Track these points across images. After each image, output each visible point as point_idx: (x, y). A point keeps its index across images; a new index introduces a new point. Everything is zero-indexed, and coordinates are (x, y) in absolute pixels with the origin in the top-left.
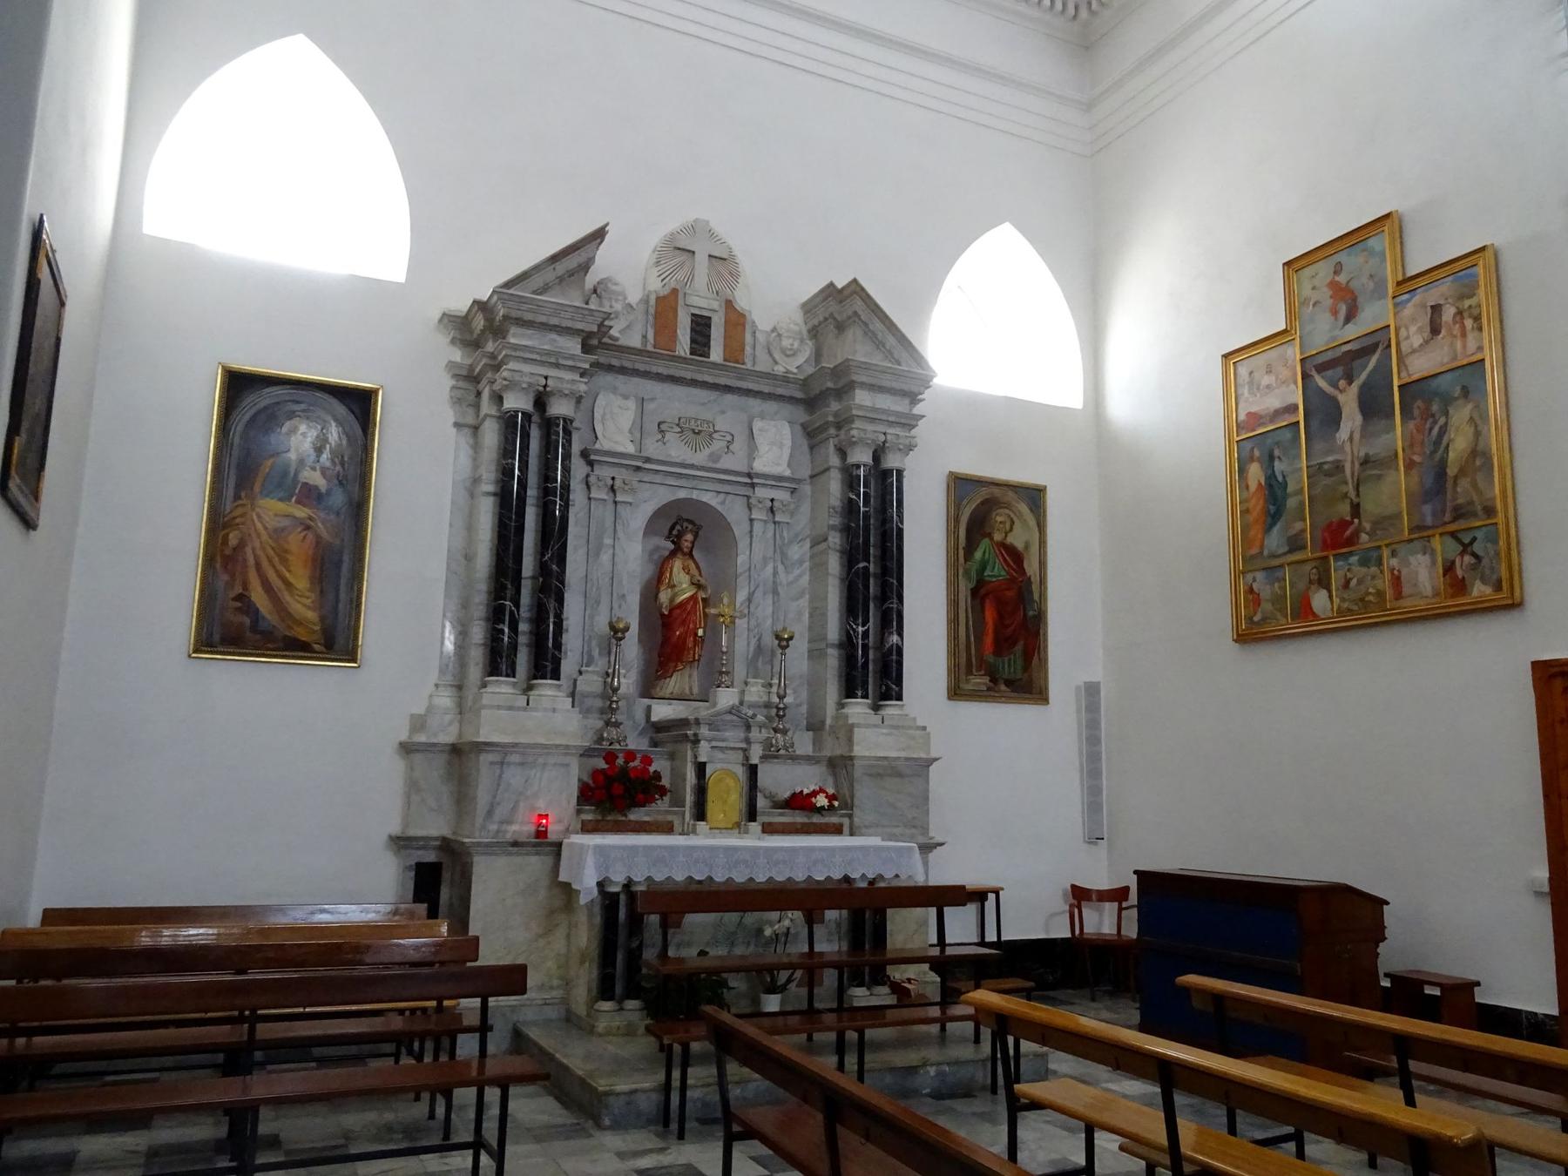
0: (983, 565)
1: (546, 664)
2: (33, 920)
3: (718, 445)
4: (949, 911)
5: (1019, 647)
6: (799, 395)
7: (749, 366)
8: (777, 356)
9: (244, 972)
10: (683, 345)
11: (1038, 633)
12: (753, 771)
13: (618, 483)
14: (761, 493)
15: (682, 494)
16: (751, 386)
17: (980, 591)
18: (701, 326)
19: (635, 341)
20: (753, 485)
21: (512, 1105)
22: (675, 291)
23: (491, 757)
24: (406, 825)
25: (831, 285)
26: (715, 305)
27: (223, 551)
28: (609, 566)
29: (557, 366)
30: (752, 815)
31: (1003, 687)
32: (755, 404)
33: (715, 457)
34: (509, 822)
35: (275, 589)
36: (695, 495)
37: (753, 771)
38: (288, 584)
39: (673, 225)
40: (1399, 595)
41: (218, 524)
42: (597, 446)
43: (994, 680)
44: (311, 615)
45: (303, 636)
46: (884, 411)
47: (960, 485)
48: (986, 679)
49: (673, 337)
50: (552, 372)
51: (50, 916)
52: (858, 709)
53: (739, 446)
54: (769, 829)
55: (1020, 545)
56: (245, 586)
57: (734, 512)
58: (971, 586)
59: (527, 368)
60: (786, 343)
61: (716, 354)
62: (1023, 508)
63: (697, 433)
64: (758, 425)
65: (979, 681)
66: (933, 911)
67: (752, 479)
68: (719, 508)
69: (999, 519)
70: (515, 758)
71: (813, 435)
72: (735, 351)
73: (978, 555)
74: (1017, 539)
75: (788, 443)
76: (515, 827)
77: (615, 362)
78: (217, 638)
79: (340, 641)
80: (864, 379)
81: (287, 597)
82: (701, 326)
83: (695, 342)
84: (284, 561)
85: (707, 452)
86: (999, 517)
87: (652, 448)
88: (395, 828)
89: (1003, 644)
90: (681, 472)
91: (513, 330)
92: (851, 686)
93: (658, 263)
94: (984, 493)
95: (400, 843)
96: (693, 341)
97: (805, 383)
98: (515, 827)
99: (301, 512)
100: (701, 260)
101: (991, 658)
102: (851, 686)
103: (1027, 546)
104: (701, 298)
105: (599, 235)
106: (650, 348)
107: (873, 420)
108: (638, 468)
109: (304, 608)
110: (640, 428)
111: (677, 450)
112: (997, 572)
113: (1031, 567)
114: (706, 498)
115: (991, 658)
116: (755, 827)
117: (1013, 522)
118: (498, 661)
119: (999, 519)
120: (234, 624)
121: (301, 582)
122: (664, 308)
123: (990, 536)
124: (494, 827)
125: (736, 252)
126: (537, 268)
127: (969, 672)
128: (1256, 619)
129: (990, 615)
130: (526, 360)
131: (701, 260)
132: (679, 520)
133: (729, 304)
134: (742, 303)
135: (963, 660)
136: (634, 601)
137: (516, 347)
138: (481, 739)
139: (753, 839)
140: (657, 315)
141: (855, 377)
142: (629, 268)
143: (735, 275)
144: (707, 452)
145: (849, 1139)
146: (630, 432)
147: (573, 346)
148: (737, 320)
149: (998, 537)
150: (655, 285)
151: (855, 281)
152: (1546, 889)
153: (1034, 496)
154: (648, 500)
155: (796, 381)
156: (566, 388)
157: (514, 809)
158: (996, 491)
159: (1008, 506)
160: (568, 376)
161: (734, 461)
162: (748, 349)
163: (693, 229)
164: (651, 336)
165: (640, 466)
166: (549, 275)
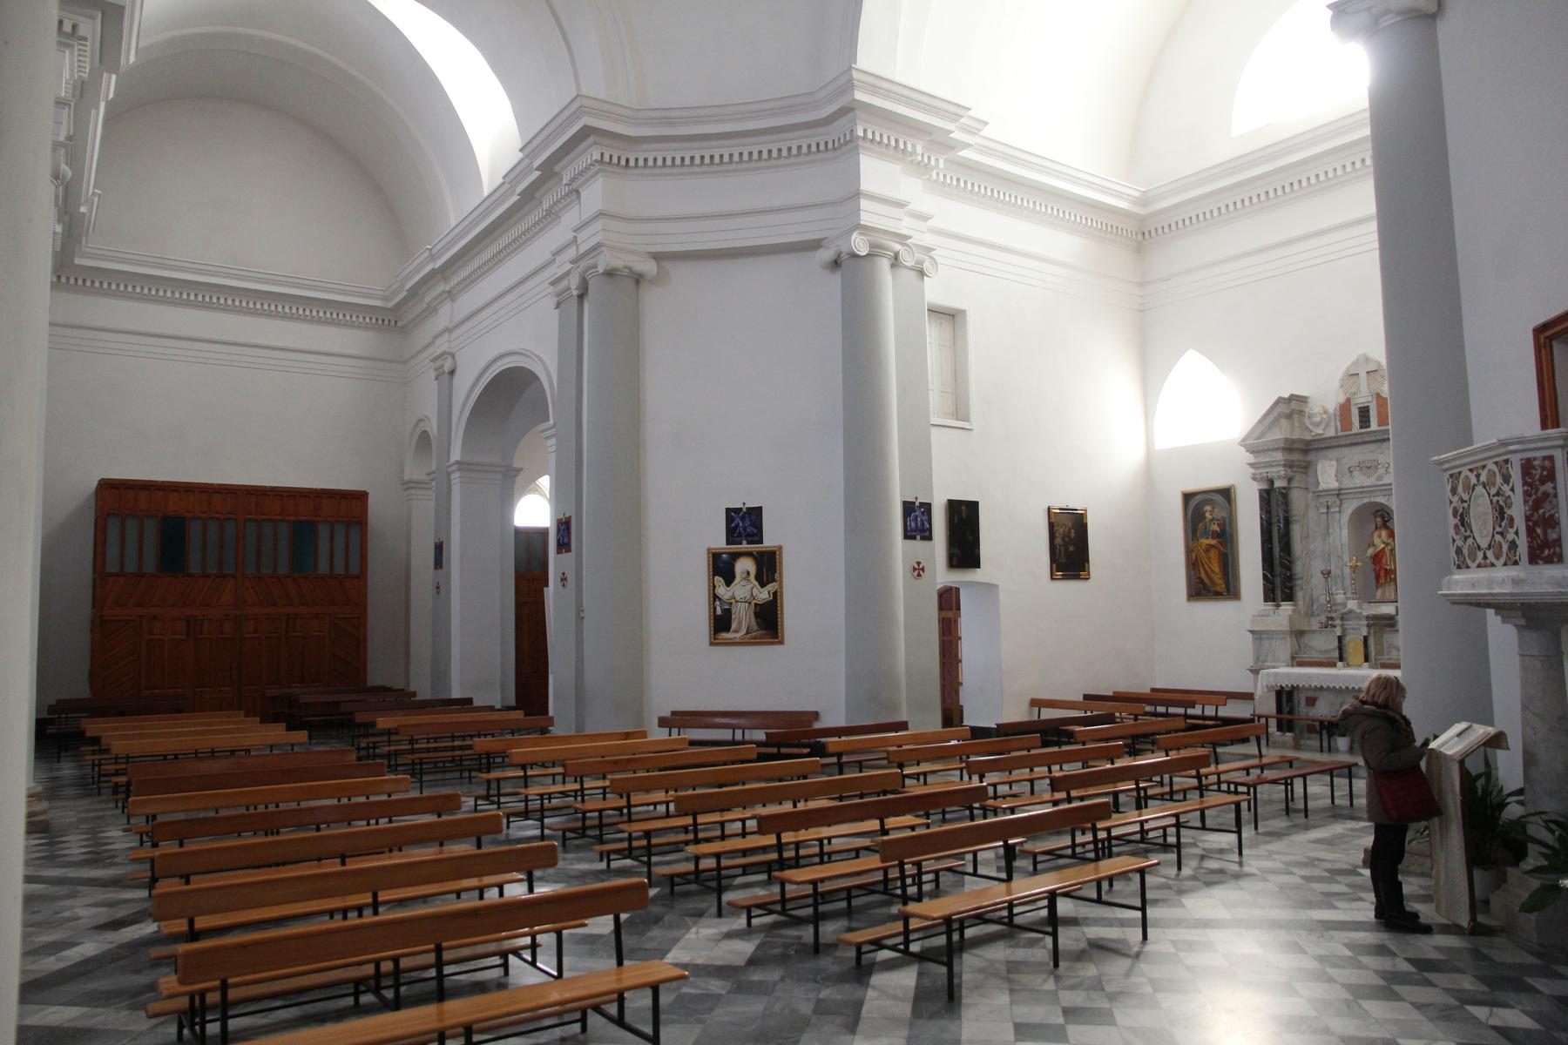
1: (1289, 597)
3: (1381, 471)
9: (805, 777)
10: (1356, 427)
18: (1364, 413)
19: (1331, 433)
21: (1309, 790)
22: (1348, 400)
25: (288, 729)
27: (1193, 564)
28: (1327, 546)
35: (1210, 576)
41: (1189, 551)
49: (1351, 423)
61: (1374, 426)
63: (1368, 468)
82: (1364, 413)
87: (1347, 483)
90: (1363, 491)
99: (1213, 542)
100: (1363, 375)
109: (1218, 579)
111: (1360, 480)
114: (1378, 500)
120: (1200, 589)
121: (1217, 569)
122: (1345, 408)
128: (560, 770)
147: (1279, 456)
150: (1342, 399)
151: (975, 504)
152: (911, 995)
154: (1350, 507)
163: (1355, 363)
165: (1339, 493)
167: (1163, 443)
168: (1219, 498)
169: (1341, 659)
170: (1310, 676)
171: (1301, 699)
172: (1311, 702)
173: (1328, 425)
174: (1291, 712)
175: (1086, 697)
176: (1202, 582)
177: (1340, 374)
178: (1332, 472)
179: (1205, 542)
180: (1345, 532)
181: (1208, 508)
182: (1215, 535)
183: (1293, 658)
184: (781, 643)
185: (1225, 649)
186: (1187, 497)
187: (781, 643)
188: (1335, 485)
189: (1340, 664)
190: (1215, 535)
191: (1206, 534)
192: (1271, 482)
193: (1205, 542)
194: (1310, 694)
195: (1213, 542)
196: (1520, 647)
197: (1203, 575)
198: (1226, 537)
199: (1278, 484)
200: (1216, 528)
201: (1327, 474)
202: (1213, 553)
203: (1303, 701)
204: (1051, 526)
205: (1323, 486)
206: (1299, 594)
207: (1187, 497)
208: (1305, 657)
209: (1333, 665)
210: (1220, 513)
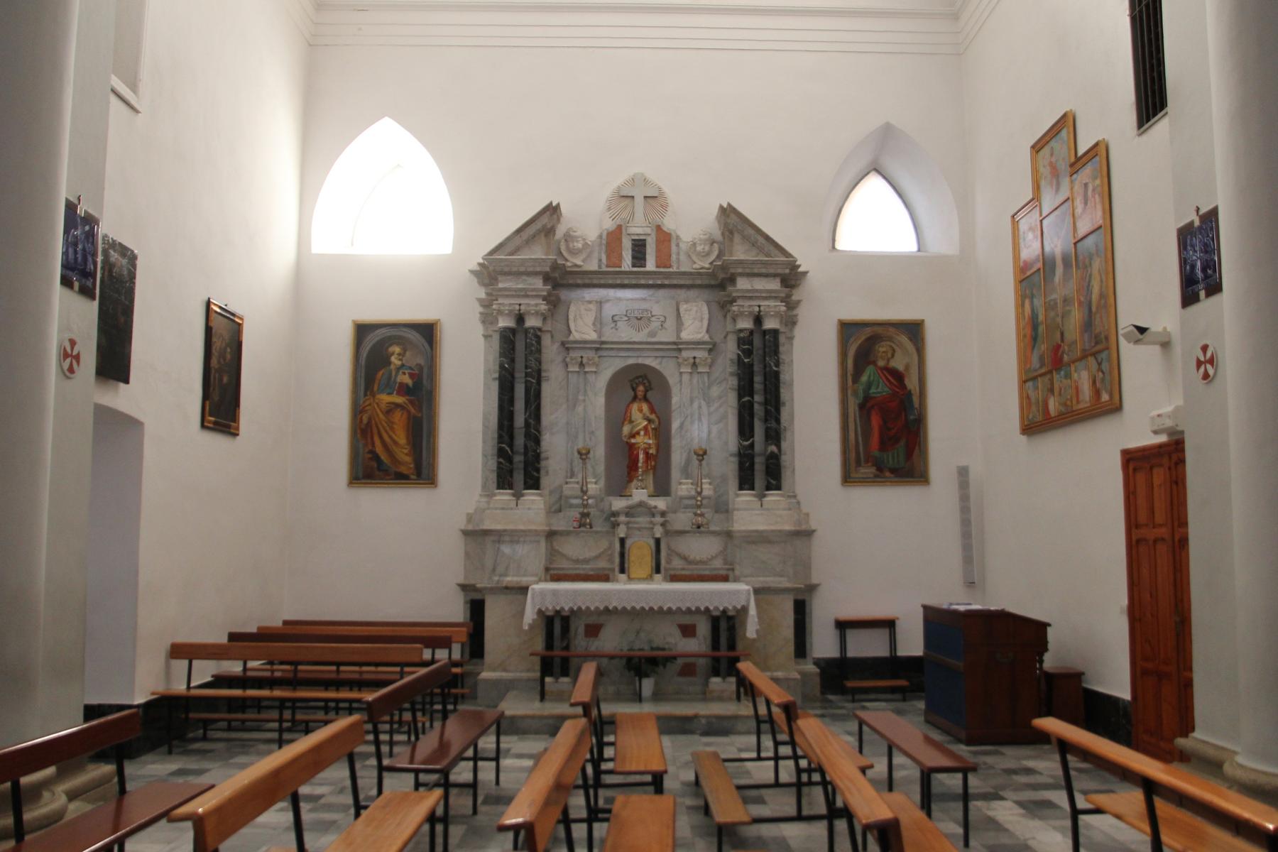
0: (869, 385)
1: (533, 483)
2: (280, 624)
3: (655, 324)
4: (195, 662)
5: (902, 443)
6: (713, 282)
7: (674, 269)
8: (694, 258)
10: (627, 263)
11: (918, 429)
12: (658, 541)
13: (585, 361)
14: (685, 354)
15: (631, 361)
16: (675, 282)
17: (866, 405)
18: (639, 248)
19: (592, 266)
20: (680, 350)
22: (619, 227)
23: (492, 538)
24: (466, 577)
26: (648, 231)
27: (364, 429)
28: (576, 417)
29: (527, 296)
30: (658, 571)
31: (888, 474)
32: (682, 293)
33: (652, 334)
34: (506, 575)
36: (640, 361)
37: (658, 541)
38: (395, 443)
39: (619, 181)
40: (1078, 402)
41: (357, 411)
42: (571, 338)
43: (880, 469)
44: (408, 459)
45: (403, 469)
46: (757, 291)
47: (847, 329)
48: (873, 470)
49: (620, 257)
50: (522, 301)
51: (286, 623)
52: (746, 497)
53: (670, 323)
54: (674, 578)
55: (901, 368)
56: (373, 444)
57: (667, 368)
58: (861, 400)
59: (507, 301)
60: (699, 248)
61: (651, 265)
62: (904, 339)
64: (683, 307)
65: (869, 470)
66: (186, 662)
67: (677, 347)
68: (658, 367)
69: (882, 350)
70: (507, 538)
71: (725, 306)
72: (663, 260)
73: (864, 378)
74: (898, 363)
75: (706, 316)
76: (509, 579)
77: (579, 281)
78: (360, 475)
79: (425, 471)
80: (740, 270)
81: (395, 449)
82: (639, 248)
83: (638, 257)
84: (392, 429)
85: (646, 331)
86: (882, 348)
87: (609, 335)
88: (461, 580)
89: (887, 443)
90: (630, 347)
91: (500, 278)
92: (746, 482)
93: (609, 209)
94: (868, 332)
95: (464, 587)
96: (634, 257)
97: (713, 275)
98: (509, 579)
99: (400, 400)
100: (639, 200)
101: (876, 453)
102: (746, 482)
103: (907, 367)
104: (639, 227)
105: (208, 303)
106: (604, 269)
107: (750, 298)
108: (597, 349)
109: (404, 455)
110: (598, 323)
111: (626, 333)
112: (881, 389)
113: (912, 383)
114: (648, 362)
115: (876, 453)
116: (658, 577)
117: (894, 351)
118: (504, 480)
119: (882, 350)
121: (402, 440)
122: (613, 239)
123: (874, 363)
124: (496, 578)
125: (666, 189)
126: (508, 239)
127: (858, 463)
129: (875, 421)
130: (507, 296)
131: (639, 200)
132: (645, 377)
133: (659, 228)
134: (669, 224)
135: (853, 455)
136: (601, 434)
137: (501, 290)
138: (485, 527)
139: (659, 585)
140: (608, 244)
141: (732, 271)
142: (587, 219)
143: (665, 207)
144: (646, 331)
145: (1159, 803)
146: (594, 324)
147: (538, 283)
148: (664, 238)
149: (881, 363)
150: (609, 225)
153: (914, 330)
154: (611, 367)
155: (707, 274)
156: (533, 310)
157: (507, 568)
158: (879, 330)
159: (890, 339)
160: (533, 302)
161: (667, 336)
162: (674, 257)
163: (632, 181)
164: (604, 260)
165: (599, 347)
166: (518, 241)
167: (323, 244)
168: (414, 336)
169: (622, 571)
170: (720, 594)
171: (578, 627)
172: (593, 631)
173: (589, 256)
174: (567, 648)
175: (233, 637)
176: (376, 458)
177: (607, 192)
178: (589, 318)
179: (385, 398)
180: (601, 400)
181: (397, 349)
182: (403, 390)
183: (547, 569)
184: (923, 321)
185: (395, 559)
186: (362, 330)
187: (923, 321)
188: (593, 336)
189: (623, 576)
190: (403, 390)
191: (389, 387)
192: (520, 319)
193: (385, 398)
194: (593, 620)
195: (400, 400)
196: (1187, 534)
197: (379, 449)
198: (421, 394)
199: (531, 322)
200: (406, 379)
201: (585, 317)
202: (398, 417)
203: (581, 630)
204: (209, 331)
205: (576, 336)
206: (544, 481)
207: (362, 330)
208: (563, 565)
209: (605, 578)
210: (413, 359)
